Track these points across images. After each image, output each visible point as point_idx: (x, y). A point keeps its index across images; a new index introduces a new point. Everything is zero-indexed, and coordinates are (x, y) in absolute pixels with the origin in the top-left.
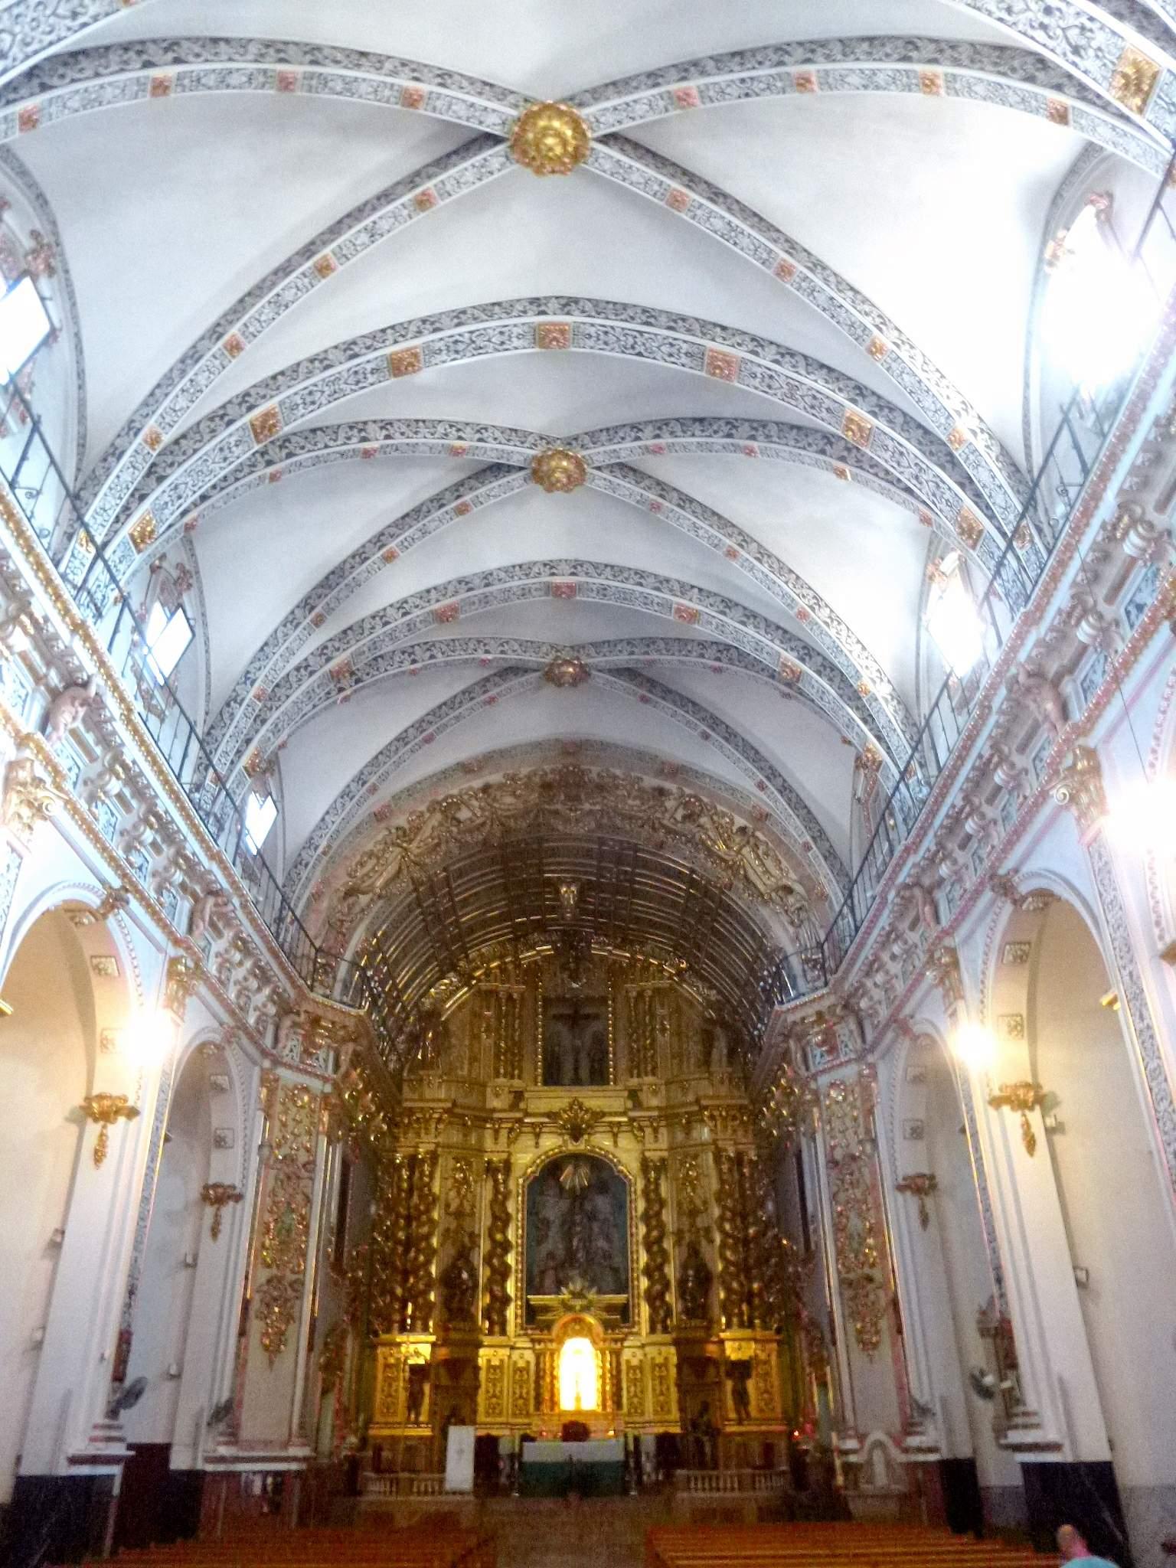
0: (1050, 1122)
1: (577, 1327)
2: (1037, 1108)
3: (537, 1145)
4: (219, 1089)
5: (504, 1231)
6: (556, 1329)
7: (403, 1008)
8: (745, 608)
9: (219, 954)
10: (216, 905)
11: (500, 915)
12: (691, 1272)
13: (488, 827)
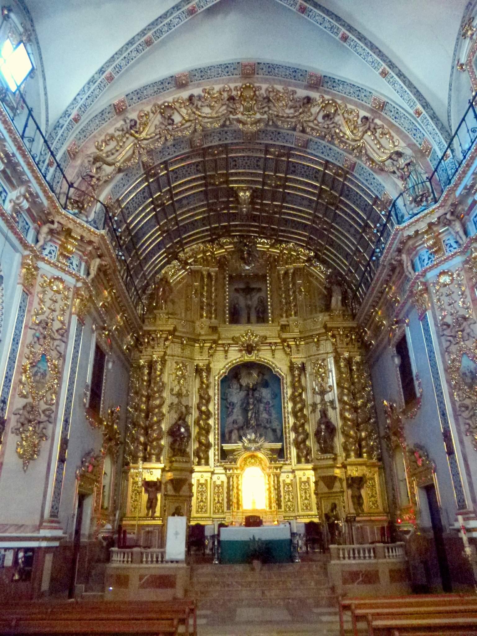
1: (253, 461)
5: (207, 405)
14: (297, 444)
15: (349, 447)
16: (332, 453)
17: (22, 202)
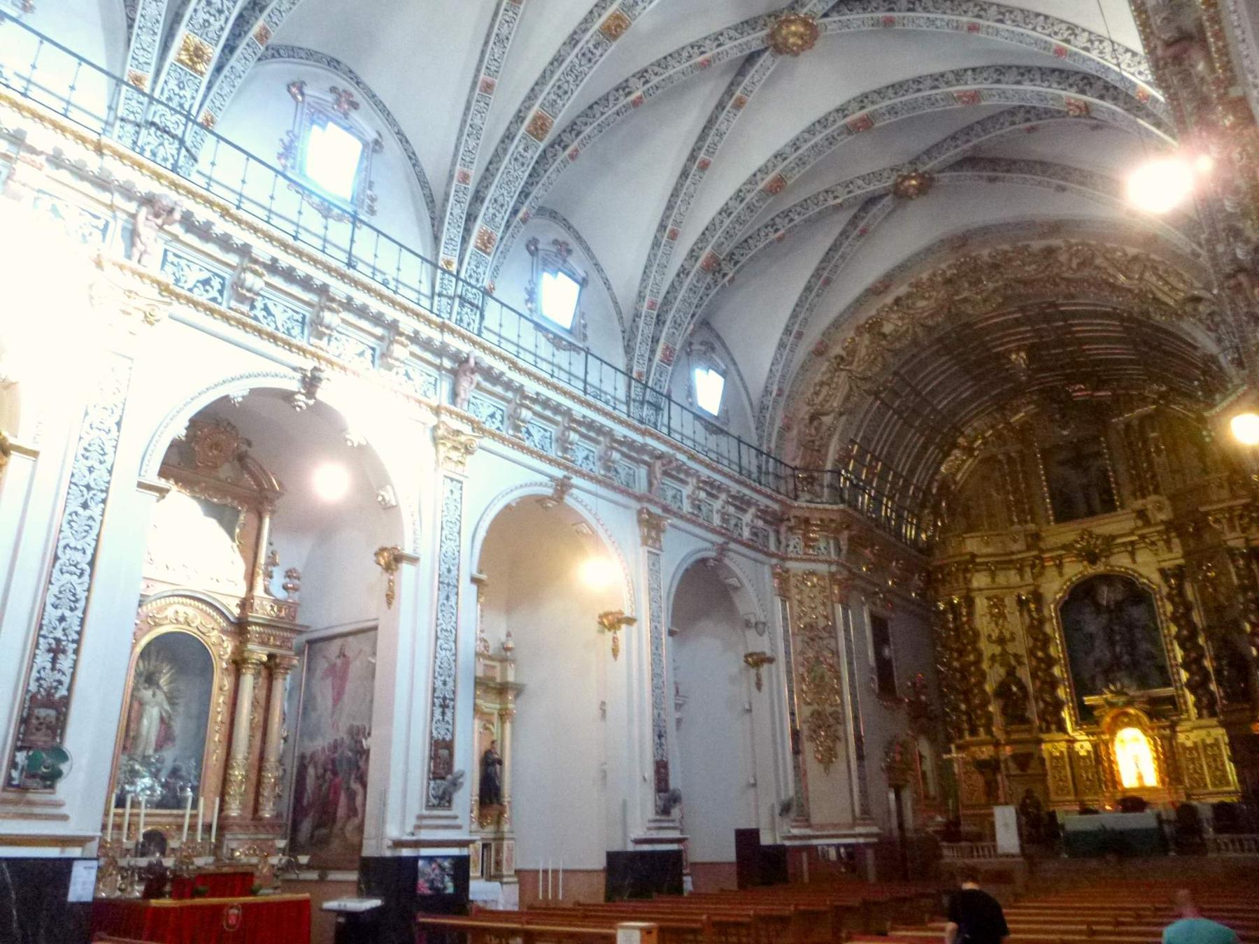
4: (736, 589)
5: (1045, 647)
8: (1018, 67)
9: (689, 497)
10: (663, 465)
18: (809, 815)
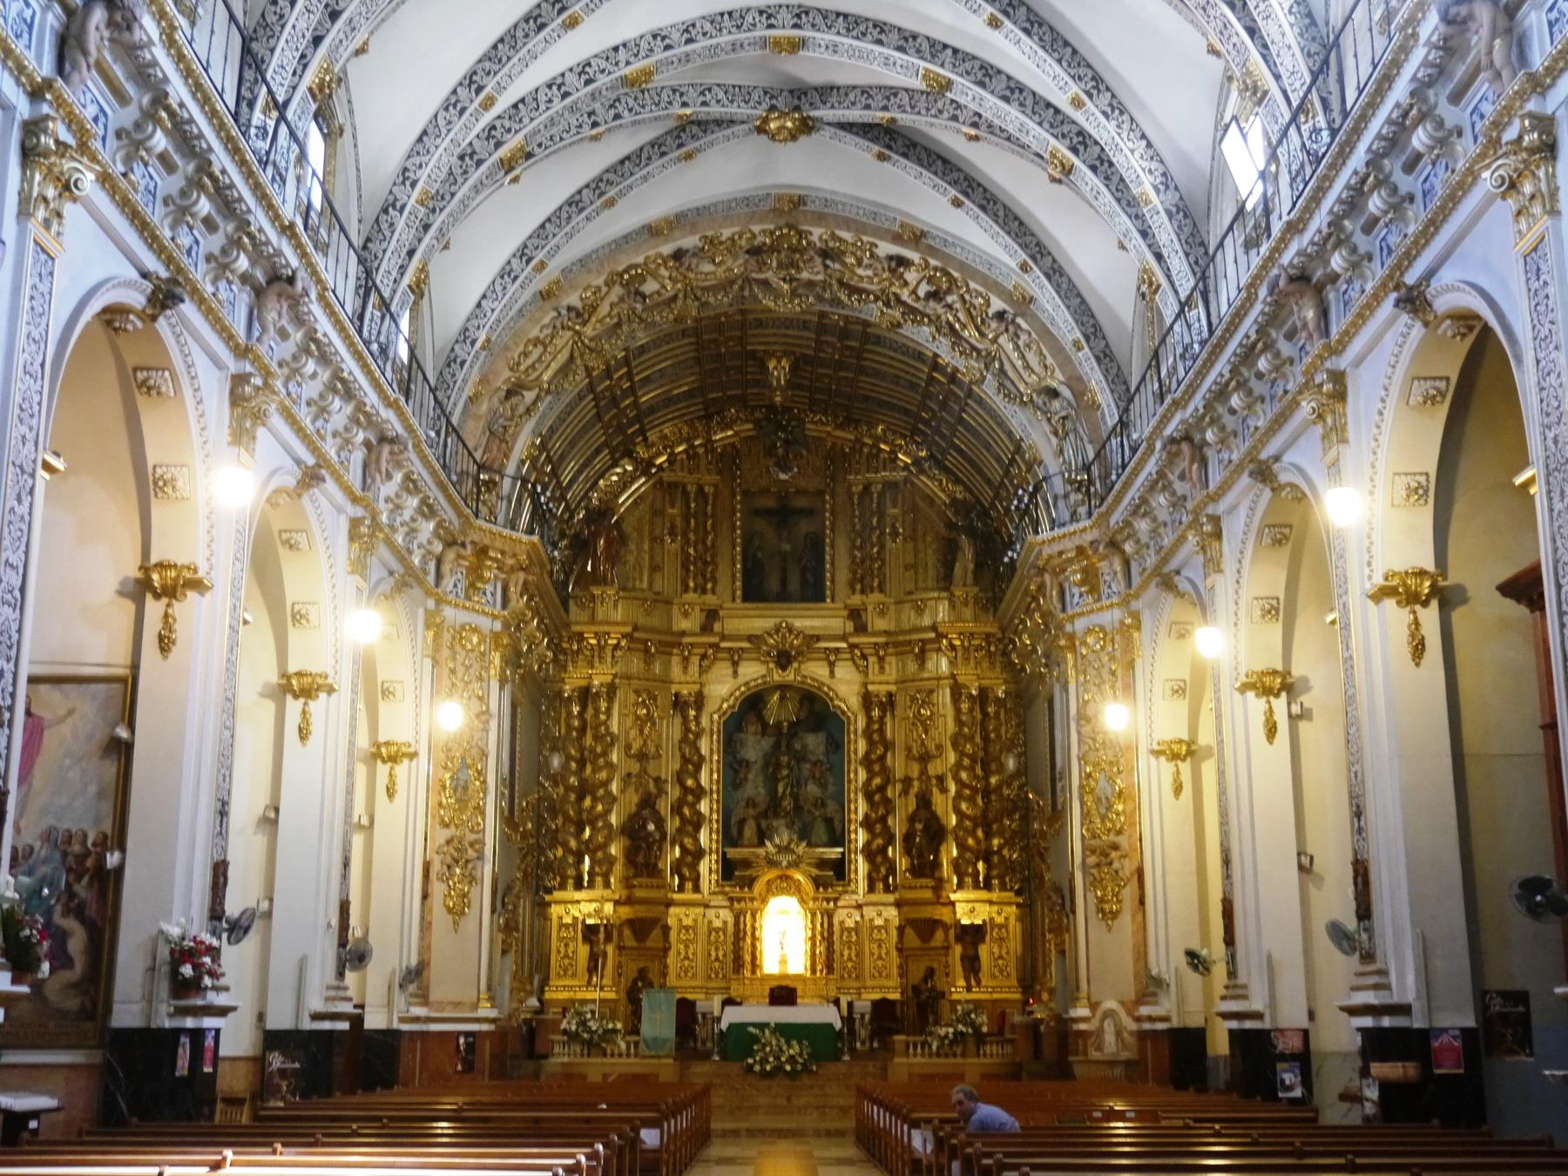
0: (1296, 709)
2: (1284, 695)
3: (735, 674)
5: (696, 775)
6: (759, 887)
7: (567, 506)
11: (688, 391)
12: (919, 826)
13: (680, 302)
14: (869, 854)
15: (963, 869)
16: (932, 877)
17: (151, 136)
18: (427, 987)
